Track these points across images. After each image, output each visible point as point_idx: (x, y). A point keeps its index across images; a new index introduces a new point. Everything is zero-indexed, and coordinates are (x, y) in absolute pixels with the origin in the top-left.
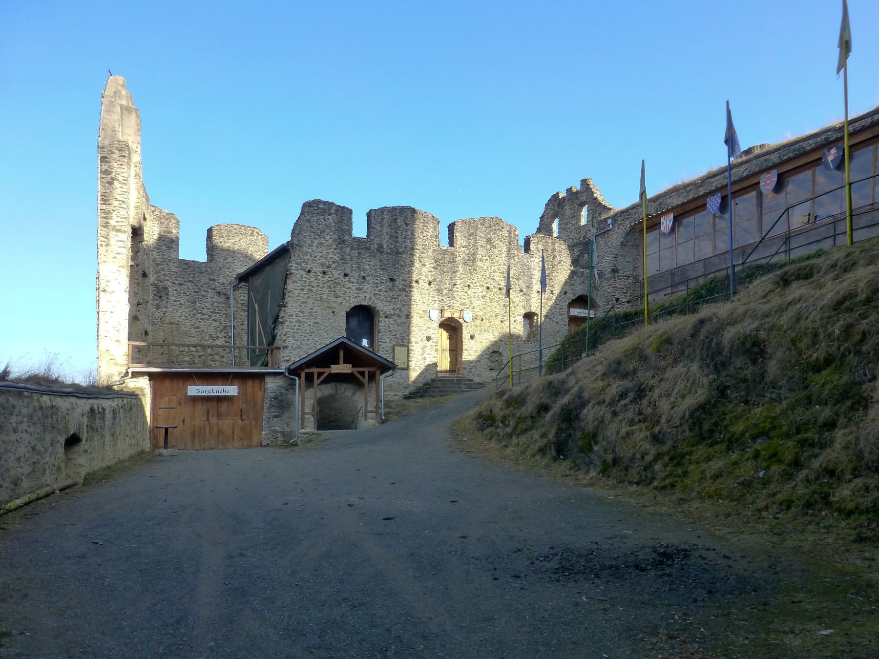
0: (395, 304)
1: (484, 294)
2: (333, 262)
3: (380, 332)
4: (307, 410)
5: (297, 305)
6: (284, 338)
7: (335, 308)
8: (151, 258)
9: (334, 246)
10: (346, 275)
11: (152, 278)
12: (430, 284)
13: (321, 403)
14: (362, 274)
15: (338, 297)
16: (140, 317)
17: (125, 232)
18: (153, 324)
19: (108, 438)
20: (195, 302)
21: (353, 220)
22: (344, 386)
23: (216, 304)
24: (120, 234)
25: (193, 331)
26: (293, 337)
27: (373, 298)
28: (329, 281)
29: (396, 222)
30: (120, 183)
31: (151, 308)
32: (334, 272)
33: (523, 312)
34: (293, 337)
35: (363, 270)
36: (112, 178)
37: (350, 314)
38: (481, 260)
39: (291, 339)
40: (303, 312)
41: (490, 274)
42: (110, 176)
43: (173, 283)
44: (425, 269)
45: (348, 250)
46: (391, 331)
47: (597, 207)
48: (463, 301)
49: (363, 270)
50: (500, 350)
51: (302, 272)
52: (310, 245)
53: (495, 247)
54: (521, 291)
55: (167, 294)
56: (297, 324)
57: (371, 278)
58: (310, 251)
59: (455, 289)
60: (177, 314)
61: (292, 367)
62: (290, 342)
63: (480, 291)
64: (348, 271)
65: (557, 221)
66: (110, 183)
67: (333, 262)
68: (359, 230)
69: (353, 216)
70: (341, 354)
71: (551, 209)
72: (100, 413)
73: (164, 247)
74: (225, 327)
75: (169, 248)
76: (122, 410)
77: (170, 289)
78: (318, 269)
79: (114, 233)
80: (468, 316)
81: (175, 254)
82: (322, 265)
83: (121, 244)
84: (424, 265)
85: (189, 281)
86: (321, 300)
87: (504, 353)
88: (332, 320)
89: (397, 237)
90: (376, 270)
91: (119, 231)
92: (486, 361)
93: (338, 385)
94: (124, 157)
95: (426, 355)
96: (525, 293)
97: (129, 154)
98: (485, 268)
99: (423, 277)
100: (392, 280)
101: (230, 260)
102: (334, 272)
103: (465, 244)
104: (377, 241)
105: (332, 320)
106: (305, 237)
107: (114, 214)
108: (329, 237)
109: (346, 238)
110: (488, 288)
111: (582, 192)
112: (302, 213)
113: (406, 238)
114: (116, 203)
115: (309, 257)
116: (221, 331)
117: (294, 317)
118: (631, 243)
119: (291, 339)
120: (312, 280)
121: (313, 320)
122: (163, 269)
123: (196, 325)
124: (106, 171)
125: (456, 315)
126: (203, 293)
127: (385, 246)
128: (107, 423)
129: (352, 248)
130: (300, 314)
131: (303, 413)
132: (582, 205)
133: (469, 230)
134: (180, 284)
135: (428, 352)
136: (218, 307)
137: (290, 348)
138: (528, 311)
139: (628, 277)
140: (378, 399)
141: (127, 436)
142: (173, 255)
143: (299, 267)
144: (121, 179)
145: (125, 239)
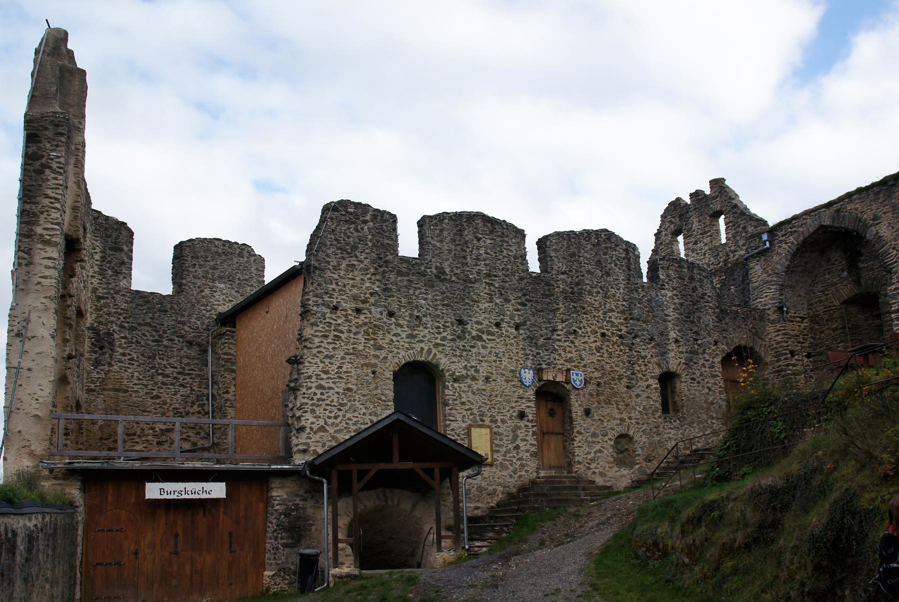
0: (468, 360)
1: (599, 344)
2: (371, 294)
3: (447, 405)
4: (341, 536)
5: (317, 360)
6: (298, 414)
7: (375, 365)
8: (90, 287)
9: (372, 270)
10: (391, 314)
11: (90, 319)
12: (517, 328)
13: (360, 522)
14: (416, 313)
15: (380, 348)
16: (71, 379)
17: (56, 244)
18: (90, 391)
19: (19, 583)
20: (154, 357)
21: (399, 231)
22: (397, 492)
23: (185, 361)
24: (48, 249)
25: (149, 402)
26: (313, 411)
27: (434, 351)
28: (365, 324)
29: (461, 235)
30: (54, 171)
31: (87, 366)
32: (373, 309)
33: (658, 371)
34: (313, 411)
35: (417, 307)
36: (42, 165)
37: (398, 376)
38: (590, 293)
39: (308, 416)
40: (326, 372)
41: (604, 314)
42: (39, 163)
43: (122, 327)
44: (509, 307)
45: (392, 277)
46: (463, 403)
47: (741, 216)
48: (570, 355)
49: (417, 307)
50: (631, 433)
51: (325, 310)
52: (335, 268)
53: (608, 274)
54: (652, 339)
55: (112, 344)
56: (319, 392)
57: (429, 319)
58: (336, 276)
59: (555, 337)
60: (125, 375)
61: (317, 463)
62: (308, 420)
63: (593, 341)
64: (394, 307)
65: (680, 238)
66: (40, 172)
67: (371, 294)
68: (408, 244)
69: (398, 225)
70: (395, 439)
71: (671, 222)
72: (8, 540)
73: (110, 272)
74: (199, 397)
75: (117, 273)
76: (41, 535)
77: (116, 336)
78: (349, 306)
79: (40, 246)
80: (577, 378)
81: (125, 282)
82: (355, 298)
83: (49, 263)
84: (507, 301)
85: (145, 324)
86: (355, 353)
87: (636, 438)
88: (373, 386)
89: (465, 258)
90: (435, 307)
91: (47, 243)
92: (611, 450)
93: (388, 491)
94: (62, 134)
95: (518, 442)
96: (659, 343)
97: (69, 131)
98: (597, 305)
99: (507, 319)
100: (461, 322)
101: (207, 291)
102: (373, 309)
103: (564, 268)
104: (435, 262)
105: (373, 386)
106: (327, 255)
107: (42, 217)
108: (365, 258)
109: (390, 257)
110: (603, 335)
111: (715, 198)
112: (323, 220)
113: (478, 259)
114: (46, 201)
115: (334, 286)
116: (193, 403)
117: (314, 379)
118: (800, 269)
119: (308, 416)
120: (339, 321)
121: (343, 385)
122: (106, 305)
123: (155, 393)
124: (35, 154)
125: (560, 378)
126: (165, 342)
127: (447, 270)
128: (18, 558)
129: (400, 273)
130: (325, 376)
131: (336, 541)
132: (716, 215)
133: (568, 248)
134: (132, 329)
135: (521, 436)
136: (188, 364)
137: (308, 430)
138: (665, 370)
139: (803, 319)
140: (457, 509)
141: (47, 580)
142: (123, 284)
143: (320, 301)
144: (54, 165)
145: (55, 255)
